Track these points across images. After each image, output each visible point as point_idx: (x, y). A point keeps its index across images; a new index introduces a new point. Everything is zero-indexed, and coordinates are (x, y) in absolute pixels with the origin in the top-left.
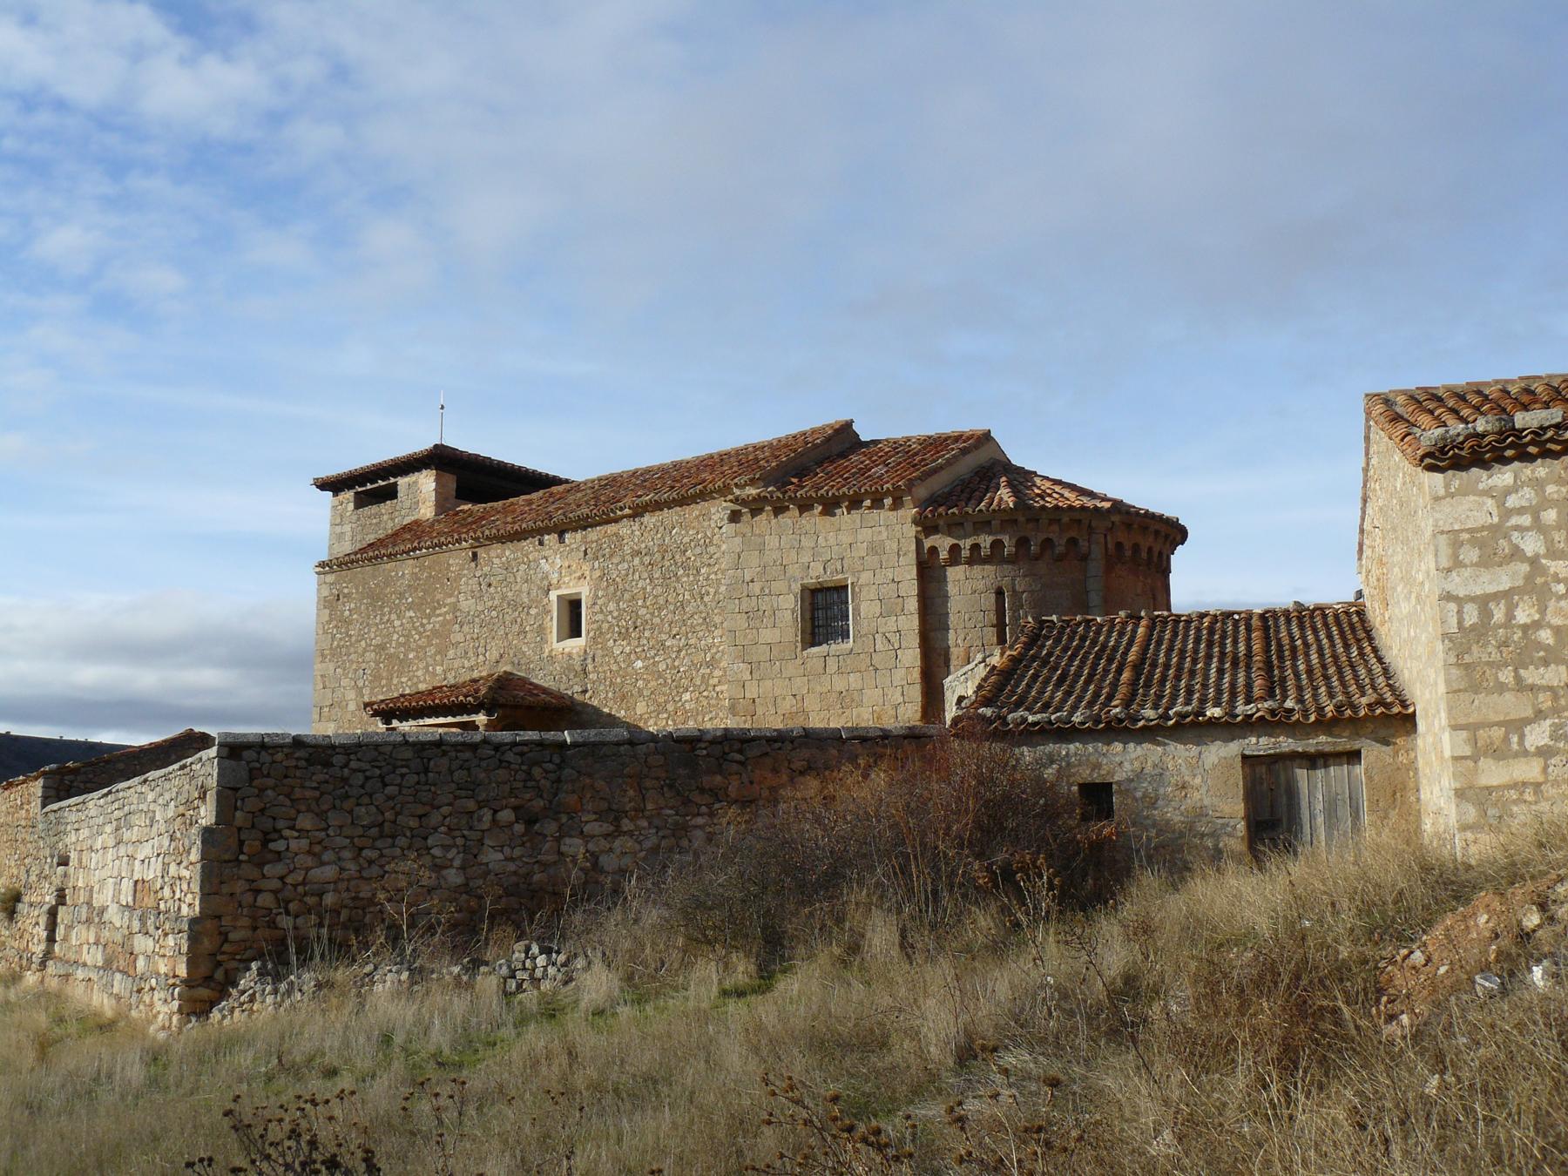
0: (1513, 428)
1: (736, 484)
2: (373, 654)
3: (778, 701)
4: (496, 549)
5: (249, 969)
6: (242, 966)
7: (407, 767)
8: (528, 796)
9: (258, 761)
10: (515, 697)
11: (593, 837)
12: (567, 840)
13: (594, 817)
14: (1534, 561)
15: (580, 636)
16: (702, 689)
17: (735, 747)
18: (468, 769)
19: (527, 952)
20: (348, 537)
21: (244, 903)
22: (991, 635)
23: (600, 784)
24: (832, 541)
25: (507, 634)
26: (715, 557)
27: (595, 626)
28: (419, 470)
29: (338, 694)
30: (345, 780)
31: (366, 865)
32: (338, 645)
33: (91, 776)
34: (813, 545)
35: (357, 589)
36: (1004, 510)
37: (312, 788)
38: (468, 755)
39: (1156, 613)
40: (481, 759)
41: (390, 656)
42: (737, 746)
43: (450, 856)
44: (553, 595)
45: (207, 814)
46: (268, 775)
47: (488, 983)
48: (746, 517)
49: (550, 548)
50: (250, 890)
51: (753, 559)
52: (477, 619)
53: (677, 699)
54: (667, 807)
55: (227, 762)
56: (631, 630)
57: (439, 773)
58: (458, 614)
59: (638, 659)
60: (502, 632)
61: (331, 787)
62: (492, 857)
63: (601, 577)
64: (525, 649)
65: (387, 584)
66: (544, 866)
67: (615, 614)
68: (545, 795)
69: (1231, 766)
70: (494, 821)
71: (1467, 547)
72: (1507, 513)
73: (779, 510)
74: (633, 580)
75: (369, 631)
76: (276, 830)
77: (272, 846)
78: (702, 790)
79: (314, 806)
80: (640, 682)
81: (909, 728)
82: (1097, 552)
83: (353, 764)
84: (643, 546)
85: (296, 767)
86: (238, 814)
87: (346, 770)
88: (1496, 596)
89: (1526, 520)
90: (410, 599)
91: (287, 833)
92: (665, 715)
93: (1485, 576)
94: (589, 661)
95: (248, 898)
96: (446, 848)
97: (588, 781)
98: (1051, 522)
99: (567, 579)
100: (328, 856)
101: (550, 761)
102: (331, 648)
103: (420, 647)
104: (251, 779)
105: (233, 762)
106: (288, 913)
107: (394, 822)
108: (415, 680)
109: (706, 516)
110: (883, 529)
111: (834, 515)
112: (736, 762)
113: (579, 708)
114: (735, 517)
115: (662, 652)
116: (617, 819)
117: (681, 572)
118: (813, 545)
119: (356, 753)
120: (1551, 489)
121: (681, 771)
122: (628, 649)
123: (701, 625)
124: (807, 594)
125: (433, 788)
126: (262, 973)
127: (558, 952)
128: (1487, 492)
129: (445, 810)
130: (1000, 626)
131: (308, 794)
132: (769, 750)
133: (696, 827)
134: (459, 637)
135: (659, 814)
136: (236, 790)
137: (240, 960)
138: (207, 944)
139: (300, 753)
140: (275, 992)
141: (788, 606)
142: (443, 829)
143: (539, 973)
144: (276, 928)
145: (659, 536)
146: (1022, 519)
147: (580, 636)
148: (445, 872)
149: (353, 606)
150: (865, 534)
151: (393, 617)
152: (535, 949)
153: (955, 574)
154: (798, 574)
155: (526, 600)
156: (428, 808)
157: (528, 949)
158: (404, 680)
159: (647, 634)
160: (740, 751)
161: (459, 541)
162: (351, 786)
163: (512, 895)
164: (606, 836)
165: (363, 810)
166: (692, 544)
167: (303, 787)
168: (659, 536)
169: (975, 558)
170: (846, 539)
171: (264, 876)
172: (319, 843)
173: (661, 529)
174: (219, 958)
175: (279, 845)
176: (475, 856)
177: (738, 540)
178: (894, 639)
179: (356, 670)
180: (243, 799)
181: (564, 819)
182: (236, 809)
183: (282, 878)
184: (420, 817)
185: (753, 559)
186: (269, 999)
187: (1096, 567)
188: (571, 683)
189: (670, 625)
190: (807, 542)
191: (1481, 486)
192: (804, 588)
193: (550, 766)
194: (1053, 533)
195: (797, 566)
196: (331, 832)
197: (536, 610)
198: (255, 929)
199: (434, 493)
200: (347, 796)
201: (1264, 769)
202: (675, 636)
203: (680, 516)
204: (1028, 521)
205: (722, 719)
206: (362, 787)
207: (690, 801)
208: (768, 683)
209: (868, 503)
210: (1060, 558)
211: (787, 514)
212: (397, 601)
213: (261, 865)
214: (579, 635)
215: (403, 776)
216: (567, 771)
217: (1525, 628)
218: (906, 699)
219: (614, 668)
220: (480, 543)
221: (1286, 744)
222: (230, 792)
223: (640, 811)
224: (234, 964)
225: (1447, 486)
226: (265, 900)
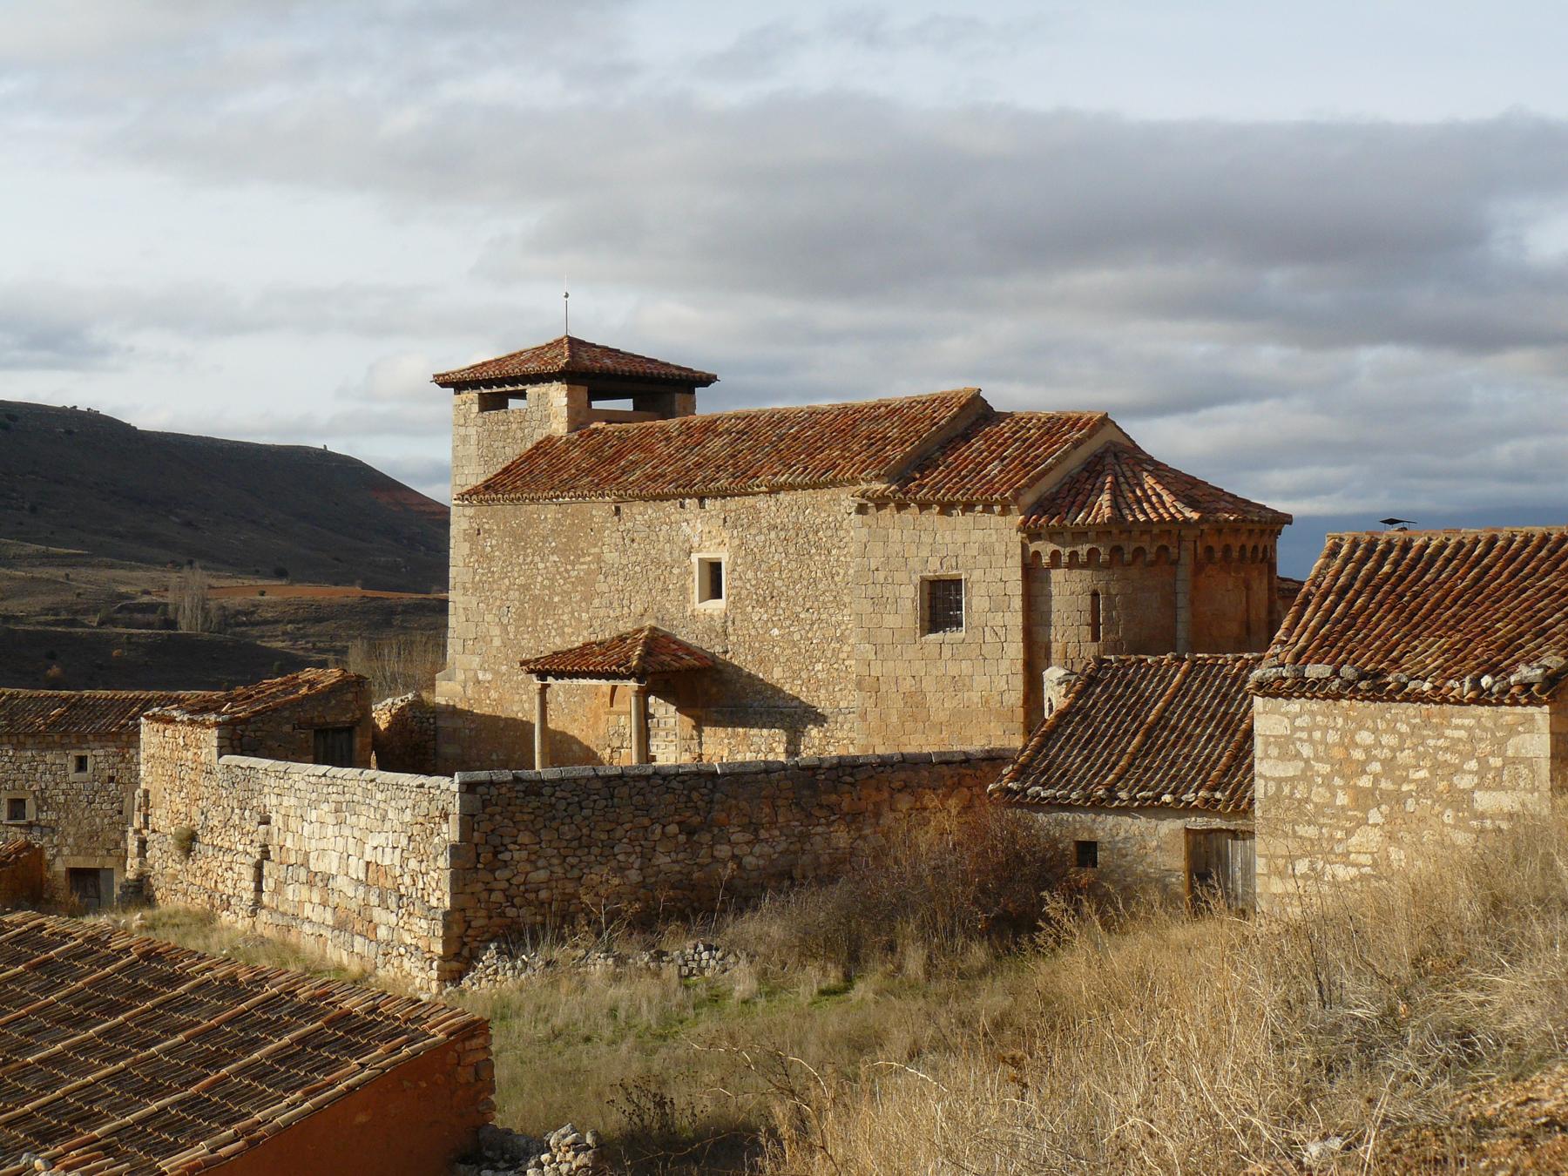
0: (1303, 677)
1: (863, 479)
2: (517, 593)
3: (900, 681)
4: (638, 507)
5: (487, 948)
6: (482, 945)
7: (598, 794)
8: (688, 814)
9: (488, 794)
10: (662, 664)
11: (738, 844)
12: (719, 847)
13: (739, 829)
14: (1307, 761)
15: (720, 597)
16: (832, 662)
17: (847, 772)
18: (644, 795)
19: (695, 949)
20: (473, 440)
21: (482, 899)
22: (1086, 632)
23: (743, 804)
24: (948, 539)
25: (651, 590)
26: (844, 540)
27: (734, 591)
28: (550, 381)
29: (483, 628)
30: (552, 806)
31: (569, 868)
32: (480, 581)
33: (260, 725)
34: (931, 541)
35: (499, 527)
36: (1098, 524)
37: (529, 813)
38: (642, 784)
39: (1199, 655)
40: (654, 787)
41: (535, 597)
42: (848, 771)
43: (631, 861)
44: (695, 558)
45: (450, 832)
46: (496, 805)
47: (670, 971)
48: (872, 511)
49: (691, 512)
50: (486, 890)
51: (877, 550)
52: (621, 572)
53: (810, 668)
54: (794, 820)
55: (466, 796)
56: (768, 599)
57: (622, 798)
58: (603, 565)
59: (774, 627)
60: (646, 588)
61: (543, 812)
62: (662, 860)
63: (740, 546)
64: (668, 605)
65: (529, 525)
66: (701, 867)
67: (754, 582)
68: (701, 813)
69: (1177, 836)
70: (663, 832)
71: (1272, 746)
72: (1295, 729)
73: (901, 507)
74: (770, 552)
75: (513, 570)
76: (502, 845)
77: (500, 856)
78: (821, 806)
79: (530, 825)
80: (777, 649)
81: (988, 751)
82: (1186, 559)
83: (558, 794)
84: (779, 521)
85: (517, 797)
86: (475, 834)
87: (553, 799)
88: (1286, 780)
89: (1304, 735)
90: (553, 544)
91: (511, 847)
92: (799, 682)
93: (1281, 766)
94: (729, 623)
95: (484, 895)
96: (628, 854)
97: (734, 802)
98: (1142, 533)
99: (707, 544)
100: (541, 863)
101: (705, 787)
102: (473, 582)
103: (565, 592)
104: (484, 807)
105: (470, 796)
106: (513, 905)
107: (589, 836)
108: (561, 623)
109: (836, 501)
110: (993, 532)
111: (951, 515)
112: (848, 783)
113: (720, 667)
114: (862, 510)
115: (796, 623)
116: (756, 831)
117: (813, 551)
118: (931, 541)
119: (560, 786)
120: (1319, 718)
121: (806, 792)
122: (765, 617)
123: (832, 602)
124: (927, 585)
125: (618, 810)
126: (500, 952)
127: (717, 950)
128: (1285, 714)
129: (627, 826)
130: (1095, 625)
131: (526, 817)
132: (873, 773)
133: (816, 834)
134: (602, 587)
135: (788, 825)
136: (473, 816)
137: (480, 941)
138: (456, 930)
139: (519, 787)
140: (514, 968)
141: (909, 596)
142: (625, 840)
143: (704, 963)
144: (506, 917)
145: (794, 513)
146: (1115, 531)
147: (720, 597)
148: (627, 872)
149: (494, 542)
150: (977, 535)
151: (537, 559)
152: (701, 947)
153: (1057, 575)
154: (918, 567)
155: (669, 559)
156: (614, 825)
157: (696, 947)
158: (549, 622)
159: (783, 605)
160: (851, 775)
161: (603, 495)
162: (556, 810)
163: (677, 888)
164: (747, 843)
165: (567, 828)
166: (824, 526)
167: (521, 812)
168: (794, 513)
169: (1073, 563)
170: (960, 539)
171: (495, 879)
172: (535, 853)
173: (795, 508)
174: (466, 940)
175: (506, 856)
176: (650, 860)
177: (865, 530)
178: (1001, 632)
179: (500, 607)
180: (478, 823)
181: (716, 831)
182: (474, 830)
183: (508, 880)
184: (608, 831)
185: (877, 550)
186: (509, 973)
187: (1184, 572)
188: (712, 643)
189: (804, 599)
190: (926, 538)
191: (1283, 710)
192: (923, 580)
193: (705, 791)
194: (1145, 542)
195: (916, 559)
196: (544, 846)
197: (678, 570)
198: (490, 918)
199: (566, 408)
200: (554, 818)
201: (1202, 837)
202: (808, 610)
203: (812, 498)
204: (1121, 532)
205: (850, 691)
206: (565, 810)
207: (811, 815)
208: (891, 664)
209: (980, 508)
210: (1153, 564)
211: (909, 511)
212: (540, 544)
213: (493, 871)
214: (719, 596)
215: (595, 801)
216: (718, 796)
217: (1299, 801)
218: (1010, 688)
219: (753, 632)
220: (622, 499)
221: (1217, 823)
222: (469, 818)
223: (773, 823)
224: (475, 944)
225: (1264, 707)
226: (497, 897)
